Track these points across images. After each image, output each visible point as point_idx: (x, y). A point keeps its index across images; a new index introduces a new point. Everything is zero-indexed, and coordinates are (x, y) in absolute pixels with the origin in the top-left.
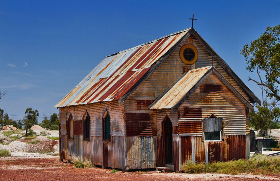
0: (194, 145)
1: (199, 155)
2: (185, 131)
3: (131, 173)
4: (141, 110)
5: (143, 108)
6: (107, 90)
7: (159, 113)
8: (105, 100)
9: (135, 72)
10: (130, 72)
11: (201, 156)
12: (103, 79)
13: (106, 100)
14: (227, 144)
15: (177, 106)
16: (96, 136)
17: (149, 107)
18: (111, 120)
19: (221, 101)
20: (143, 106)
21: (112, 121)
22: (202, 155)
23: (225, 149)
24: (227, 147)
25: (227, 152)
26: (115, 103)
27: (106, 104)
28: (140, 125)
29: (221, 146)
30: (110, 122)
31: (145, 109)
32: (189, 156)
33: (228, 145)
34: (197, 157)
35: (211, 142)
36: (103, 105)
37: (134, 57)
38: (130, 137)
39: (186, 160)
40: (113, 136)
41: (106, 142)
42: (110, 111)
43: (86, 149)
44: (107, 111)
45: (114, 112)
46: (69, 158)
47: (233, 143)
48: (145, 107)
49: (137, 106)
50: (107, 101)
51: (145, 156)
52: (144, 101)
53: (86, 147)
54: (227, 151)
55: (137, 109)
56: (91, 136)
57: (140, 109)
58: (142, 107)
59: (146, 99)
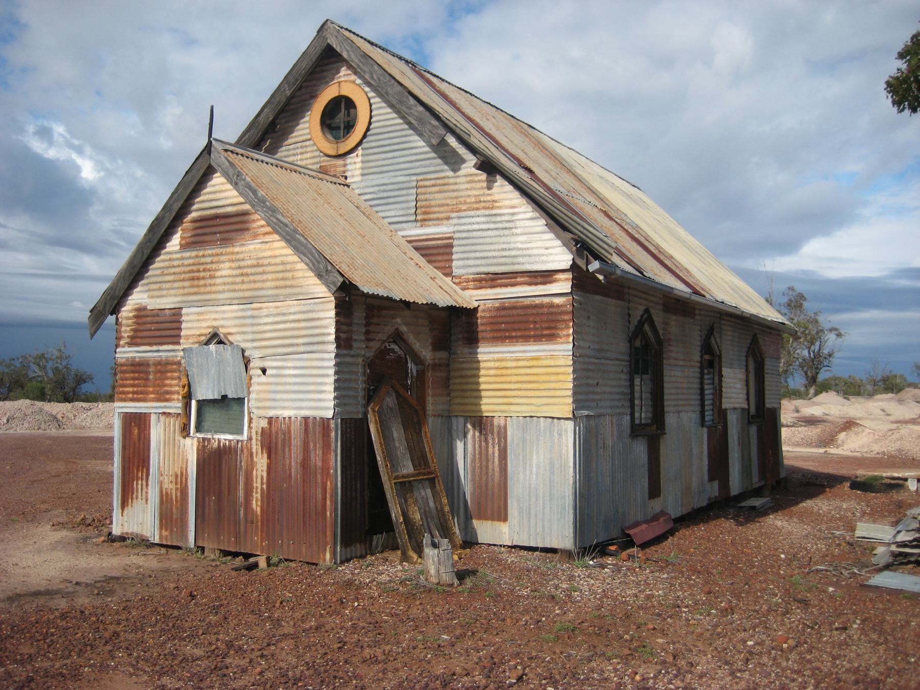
2: (133, 393)
11: (177, 489)
15: (105, 304)
19: (247, 275)
24: (261, 463)
35: (209, 440)
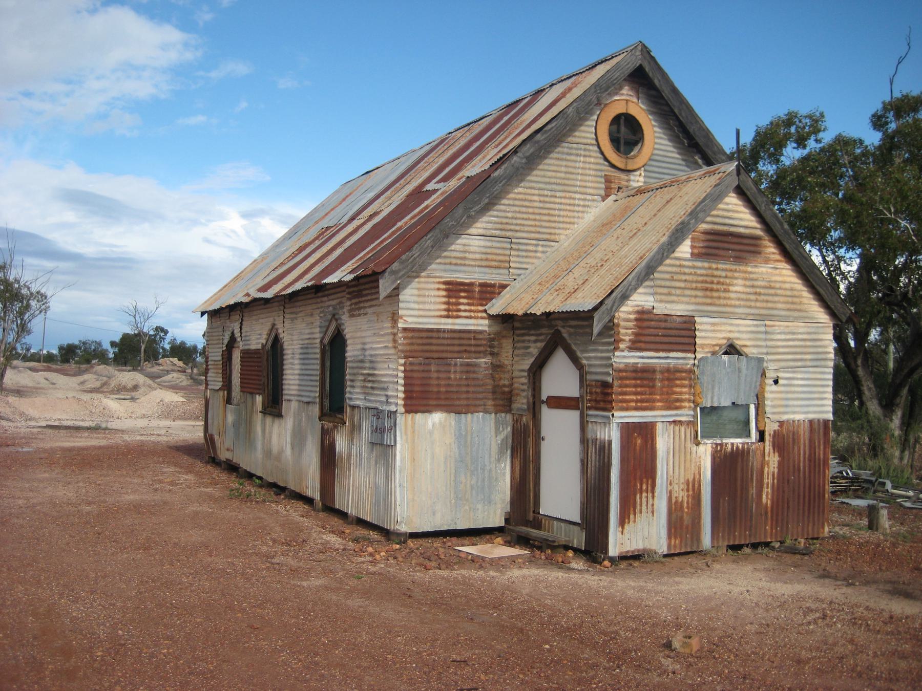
0: (665, 454)
1: (681, 494)
2: (637, 401)
4: (458, 317)
5: (465, 311)
6: (339, 251)
7: (522, 332)
8: (327, 281)
9: (435, 191)
10: (419, 194)
11: (688, 496)
12: (328, 228)
14: (772, 451)
16: (299, 401)
17: (486, 307)
18: (349, 348)
20: (468, 304)
21: (351, 352)
22: (691, 493)
23: (766, 470)
24: (773, 461)
25: (770, 481)
26: (367, 292)
27: (332, 297)
28: (455, 372)
29: (755, 462)
30: (344, 358)
31: (472, 314)
32: (647, 497)
33: (777, 454)
34: (674, 501)
35: (721, 445)
36: (325, 299)
37: (426, 162)
38: (419, 416)
39: (635, 514)
40: (353, 407)
41: (331, 425)
42: (345, 318)
43: (270, 440)
44: (337, 320)
45: (361, 322)
46: (227, 457)
47: (793, 448)
48: (473, 308)
49: (445, 303)
50: (336, 280)
51: (468, 486)
53: (271, 433)
54: (770, 476)
55: (445, 313)
56: (285, 397)
57: (455, 313)
58: (462, 307)
59: (477, 276)
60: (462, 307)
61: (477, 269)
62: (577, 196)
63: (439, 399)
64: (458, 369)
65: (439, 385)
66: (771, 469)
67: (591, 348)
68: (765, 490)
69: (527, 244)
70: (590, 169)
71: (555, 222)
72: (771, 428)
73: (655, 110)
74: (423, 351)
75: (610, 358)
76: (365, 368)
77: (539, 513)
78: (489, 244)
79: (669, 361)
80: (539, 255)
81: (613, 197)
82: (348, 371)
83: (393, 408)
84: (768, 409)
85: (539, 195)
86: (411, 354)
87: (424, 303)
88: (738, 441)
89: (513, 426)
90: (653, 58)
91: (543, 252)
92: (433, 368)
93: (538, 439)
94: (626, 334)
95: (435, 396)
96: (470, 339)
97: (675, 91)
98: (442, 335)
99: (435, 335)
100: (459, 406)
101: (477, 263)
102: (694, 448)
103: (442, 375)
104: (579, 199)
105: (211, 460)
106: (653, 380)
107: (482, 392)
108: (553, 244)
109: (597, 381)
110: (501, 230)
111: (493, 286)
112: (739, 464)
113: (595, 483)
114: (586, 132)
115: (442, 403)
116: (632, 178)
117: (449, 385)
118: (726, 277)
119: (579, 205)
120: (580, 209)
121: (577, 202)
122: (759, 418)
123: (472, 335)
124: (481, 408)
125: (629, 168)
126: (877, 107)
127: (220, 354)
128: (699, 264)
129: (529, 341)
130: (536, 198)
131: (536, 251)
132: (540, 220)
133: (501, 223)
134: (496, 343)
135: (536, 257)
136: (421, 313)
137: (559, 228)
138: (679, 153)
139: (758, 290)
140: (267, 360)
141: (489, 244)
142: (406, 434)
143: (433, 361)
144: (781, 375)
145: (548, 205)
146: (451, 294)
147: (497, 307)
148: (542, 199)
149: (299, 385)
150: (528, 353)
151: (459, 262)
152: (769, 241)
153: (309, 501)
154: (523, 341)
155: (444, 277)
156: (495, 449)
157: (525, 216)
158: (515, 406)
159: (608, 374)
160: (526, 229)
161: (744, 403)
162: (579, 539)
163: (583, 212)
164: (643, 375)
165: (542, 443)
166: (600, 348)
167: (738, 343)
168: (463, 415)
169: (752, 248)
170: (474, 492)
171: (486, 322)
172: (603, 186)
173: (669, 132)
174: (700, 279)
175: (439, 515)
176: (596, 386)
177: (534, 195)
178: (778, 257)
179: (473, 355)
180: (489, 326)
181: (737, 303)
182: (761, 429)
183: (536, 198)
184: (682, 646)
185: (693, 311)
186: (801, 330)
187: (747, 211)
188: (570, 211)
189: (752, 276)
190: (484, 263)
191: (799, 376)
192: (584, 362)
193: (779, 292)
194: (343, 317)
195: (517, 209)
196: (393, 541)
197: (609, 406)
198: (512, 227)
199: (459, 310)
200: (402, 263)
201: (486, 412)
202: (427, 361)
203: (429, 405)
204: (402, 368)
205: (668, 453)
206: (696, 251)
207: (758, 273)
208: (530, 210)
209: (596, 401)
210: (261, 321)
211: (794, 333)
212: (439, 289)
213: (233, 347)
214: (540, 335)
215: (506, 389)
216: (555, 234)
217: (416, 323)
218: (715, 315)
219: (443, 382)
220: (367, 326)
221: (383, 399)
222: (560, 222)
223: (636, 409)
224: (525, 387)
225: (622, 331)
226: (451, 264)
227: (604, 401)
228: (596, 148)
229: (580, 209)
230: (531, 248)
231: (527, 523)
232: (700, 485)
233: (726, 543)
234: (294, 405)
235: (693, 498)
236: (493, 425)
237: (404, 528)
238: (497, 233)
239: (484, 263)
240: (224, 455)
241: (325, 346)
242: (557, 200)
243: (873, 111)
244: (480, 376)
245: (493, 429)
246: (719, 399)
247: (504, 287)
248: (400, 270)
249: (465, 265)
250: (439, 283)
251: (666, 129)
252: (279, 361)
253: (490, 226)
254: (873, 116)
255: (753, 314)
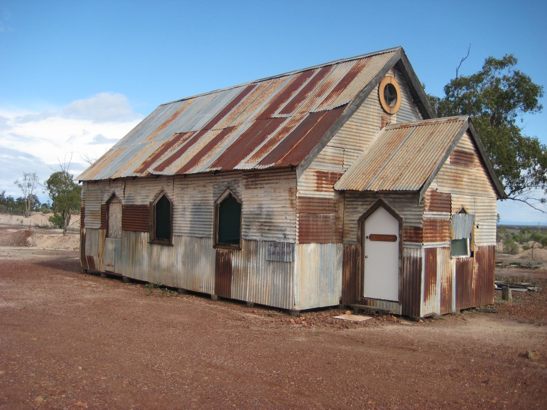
1: (445, 285)
2: (431, 237)
3: (40, 233)
4: (322, 191)
5: (325, 187)
13: (243, 165)
20: (326, 184)
24: (476, 266)
29: (470, 267)
35: (458, 259)
36: (221, 177)
38: (305, 245)
48: (328, 186)
52: (327, 173)
55: (316, 189)
58: (324, 186)
60: (324, 186)
61: (330, 165)
62: (371, 127)
63: (313, 236)
64: (322, 219)
65: (313, 228)
66: (476, 271)
67: (406, 209)
68: (473, 281)
69: (350, 152)
70: (375, 112)
71: (361, 140)
72: (476, 250)
73: (400, 82)
74: (308, 210)
75: (422, 215)
76: (261, 218)
77: (363, 297)
78: (335, 151)
79: (442, 216)
80: (355, 158)
81: (384, 128)
82: (243, 220)
83: (292, 241)
84: (475, 241)
85: (356, 126)
86: (302, 211)
87: (308, 183)
88: (464, 257)
89: (344, 250)
90: (405, 56)
91: (356, 156)
92: (311, 219)
93: (363, 257)
94: (428, 202)
95: (311, 235)
96: (326, 203)
97: (413, 73)
98: (315, 201)
99: (312, 200)
100: (321, 240)
101: (330, 161)
102: (450, 261)
103: (315, 223)
104: (371, 128)
105: (85, 272)
106: (436, 226)
107: (331, 232)
108: (361, 152)
109: (410, 227)
110: (340, 144)
111: (336, 174)
112: (465, 268)
113: (410, 280)
114: (374, 93)
115: (315, 238)
116: (392, 118)
117: (318, 228)
118: (462, 174)
119: (371, 132)
120: (371, 134)
121: (370, 130)
122: (471, 245)
123: (327, 201)
124: (330, 241)
125: (391, 113)
126: (448, 82)
127: (100, 207)
128: (453, 167)
129: (357, 205)
130: (354, 127)
131: (354, 156)
132: (356, 139)
133: (340, 140)
134: (337, 205)
135: (353, 159)
136: (307, 188)
137: (363, 144)
138: (410, 106)
139: (472, 181)
140: (154, 212)
141: (335, 151)
142: (299, 256)
143: (311, 215)
144: (480, 223)
145: (359, 131)
146: (319, 178)
147: (339, 186)
148: (357, 128)
149: (191, 227)
150: (357, 211)
151: (323, 160)
152: (476, 156)
153: (207, 296)
154: (353, 205)
155: (317, 169)
156: (336, 263)
157: (350, 137)
158: (345, 239)
159: (421, 223)
160: (351, 143)
161: (461, 238)
162: (398, 309)
163: (373, 135)
164: (433, 223)
165: (366, 259)
166: (413, 209)
167: (465, 207)
168: (323, 245)
169: (469, 159)
170: (327, 286)
171: (333, 194)
172: (381, 122)
173: (406, 95)
174: (453, 174)
175: (312, 300)
176: (410, 229)
177: (353, 125)
178: (479, 164)
179: (328, 212)
180: (334, 196)
181: (465, 187)
182: (472, 250)
183: (354, 127)
184: (534, 356)
185: (451, 191)
186: (486, 201)
187: (469, 141)
188: (367, 135)
189: (470, 173)
190: (333, 162)
191: (485, 224)
192: (402, 216)
193: (479, 182)
194: (239, 189)
195: (346, 133)
196: (294, 315)
197: (420, 240)
198: (345, 142)
199: (322, 187)
200: (305, 160)
201: (333, 243)
202: (308, 215)
203: (308, 239)
204: (298, 219)
205: (441, 263)
206: (452, 160)
207: (472, 172)
208: (352, 134)
209: (410, 237)
210: (146, 188)
211: (484, 203)
212: (314, 175)
213: (110, 203)
214: (367, 201)
215: (341, 230)
216: (361, 147)
217: (304, 194)
218: (457, 193)
219: (315, 227)
220: (264, 194)
221: (281, 236)
222: (363, 140)
223: (431, 241)
224: (355, 230)
225: (426, 201)
226: (319, 161)
227: (417, 237)
228: (378, 102)
229: (371, 134)
230: (352, 154)
231: (359, 303)
232: (452, 280)
233: (460, 309)
234: (185, 239)
235: (449, 286)
236: (335, 250)
237: (297, 308)
238: (339, 145)
239: (333, 162)
240: (102, 268)
241: (217, 204)
242: (363, 129)
243: (446, 84)
244: (330, 223)
245: (335, 252)
246: (458, 236)
247: (341, 175)
248: (305, 165)
249: (325, 162)
250: (314, 172)
251: (405, 93)
252: (171, 213)
253: (336, 141)
254: (446, 86)
255: (471, 193)
